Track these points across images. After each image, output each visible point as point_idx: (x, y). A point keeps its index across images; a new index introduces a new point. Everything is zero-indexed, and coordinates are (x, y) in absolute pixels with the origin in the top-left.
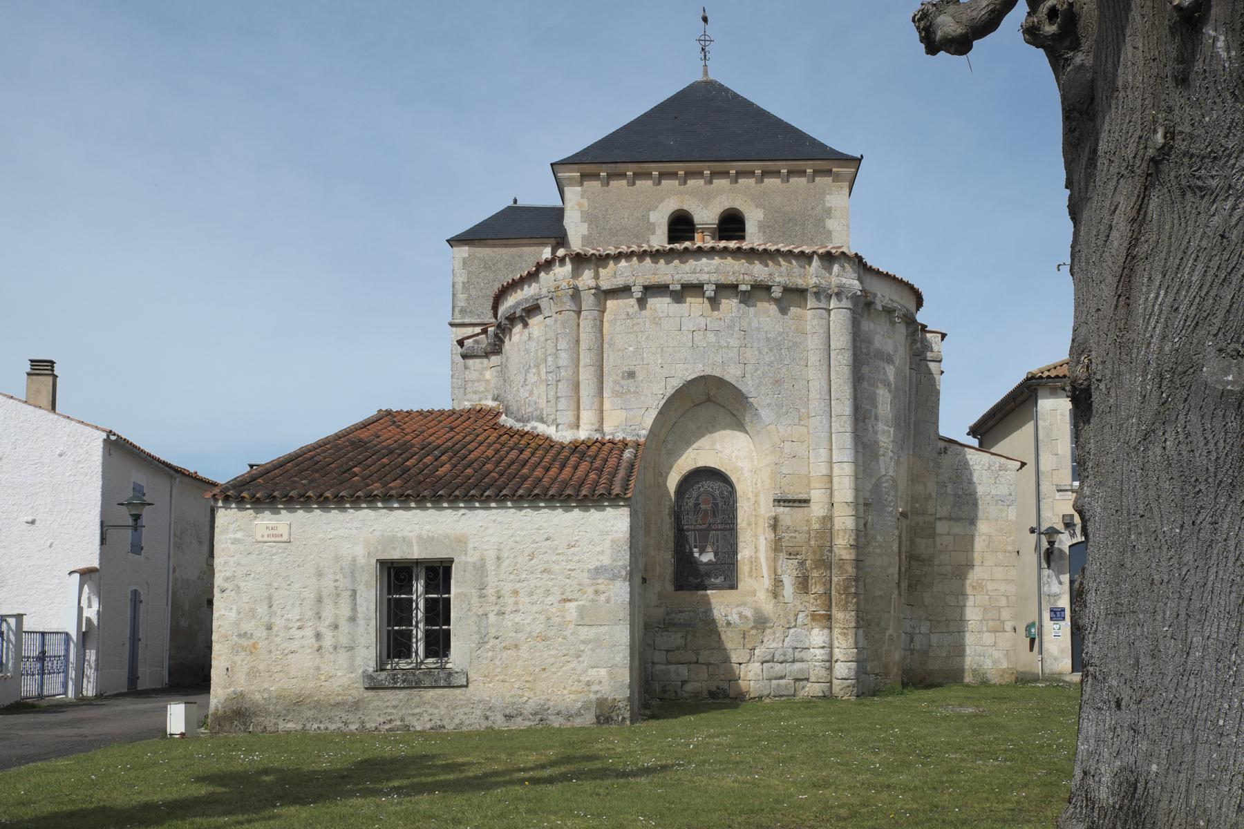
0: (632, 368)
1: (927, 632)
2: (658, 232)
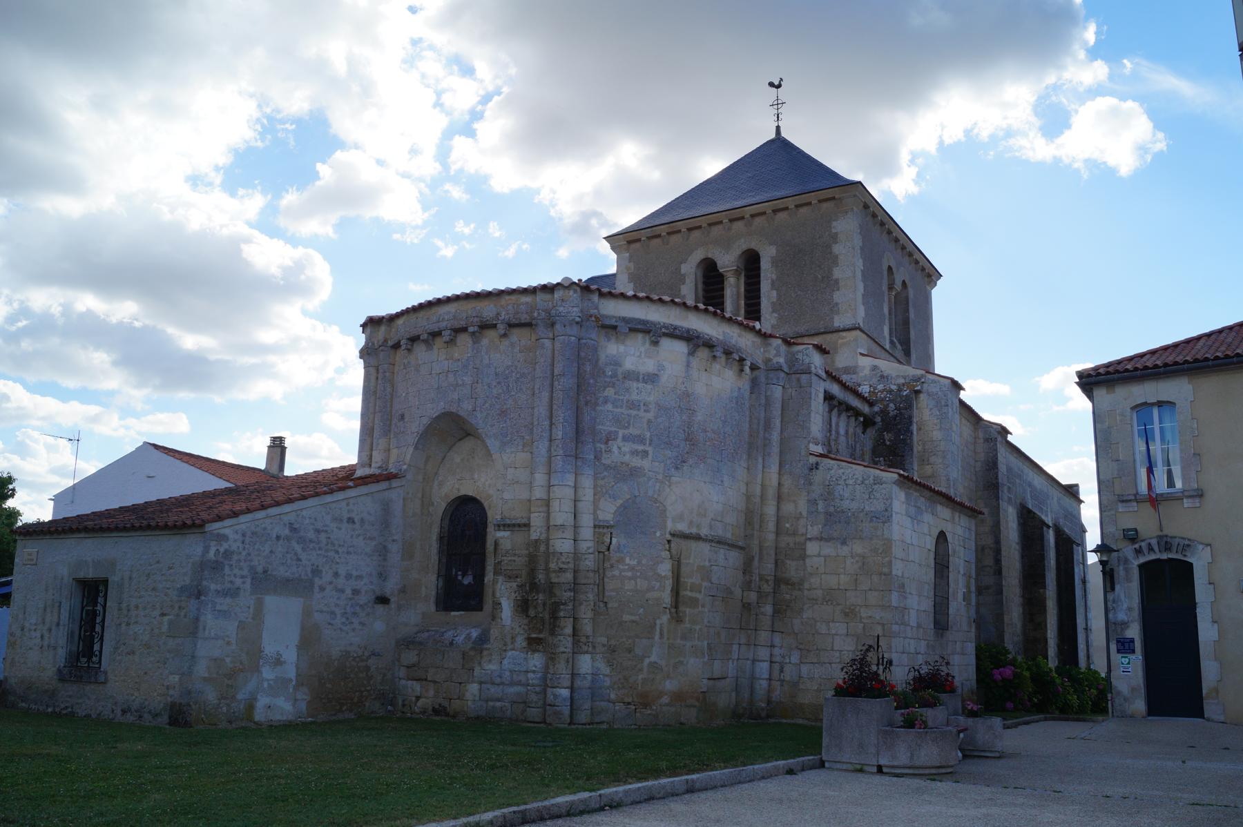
0: (403, 410)
1: (798, 662)
2: (688, 281)
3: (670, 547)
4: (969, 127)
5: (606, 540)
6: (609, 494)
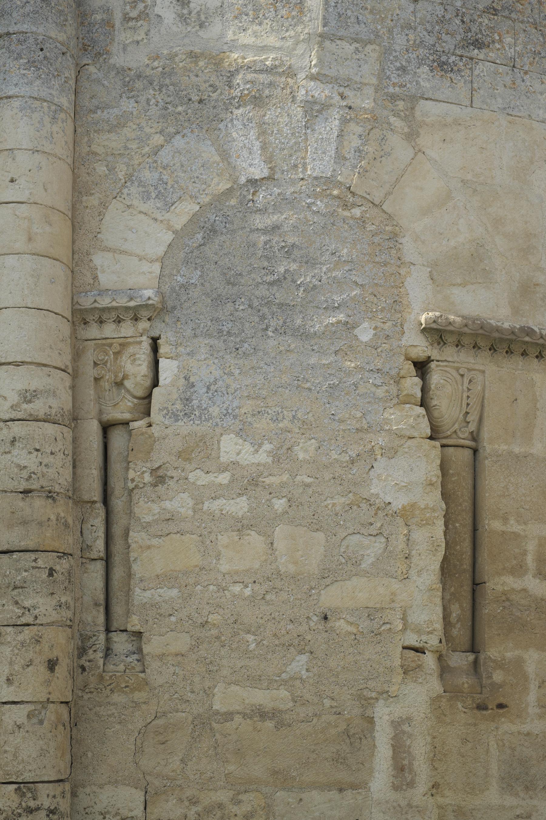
3: (424, 390)
4: (432, 358)
5: (129, 368)
6: (141, 184)
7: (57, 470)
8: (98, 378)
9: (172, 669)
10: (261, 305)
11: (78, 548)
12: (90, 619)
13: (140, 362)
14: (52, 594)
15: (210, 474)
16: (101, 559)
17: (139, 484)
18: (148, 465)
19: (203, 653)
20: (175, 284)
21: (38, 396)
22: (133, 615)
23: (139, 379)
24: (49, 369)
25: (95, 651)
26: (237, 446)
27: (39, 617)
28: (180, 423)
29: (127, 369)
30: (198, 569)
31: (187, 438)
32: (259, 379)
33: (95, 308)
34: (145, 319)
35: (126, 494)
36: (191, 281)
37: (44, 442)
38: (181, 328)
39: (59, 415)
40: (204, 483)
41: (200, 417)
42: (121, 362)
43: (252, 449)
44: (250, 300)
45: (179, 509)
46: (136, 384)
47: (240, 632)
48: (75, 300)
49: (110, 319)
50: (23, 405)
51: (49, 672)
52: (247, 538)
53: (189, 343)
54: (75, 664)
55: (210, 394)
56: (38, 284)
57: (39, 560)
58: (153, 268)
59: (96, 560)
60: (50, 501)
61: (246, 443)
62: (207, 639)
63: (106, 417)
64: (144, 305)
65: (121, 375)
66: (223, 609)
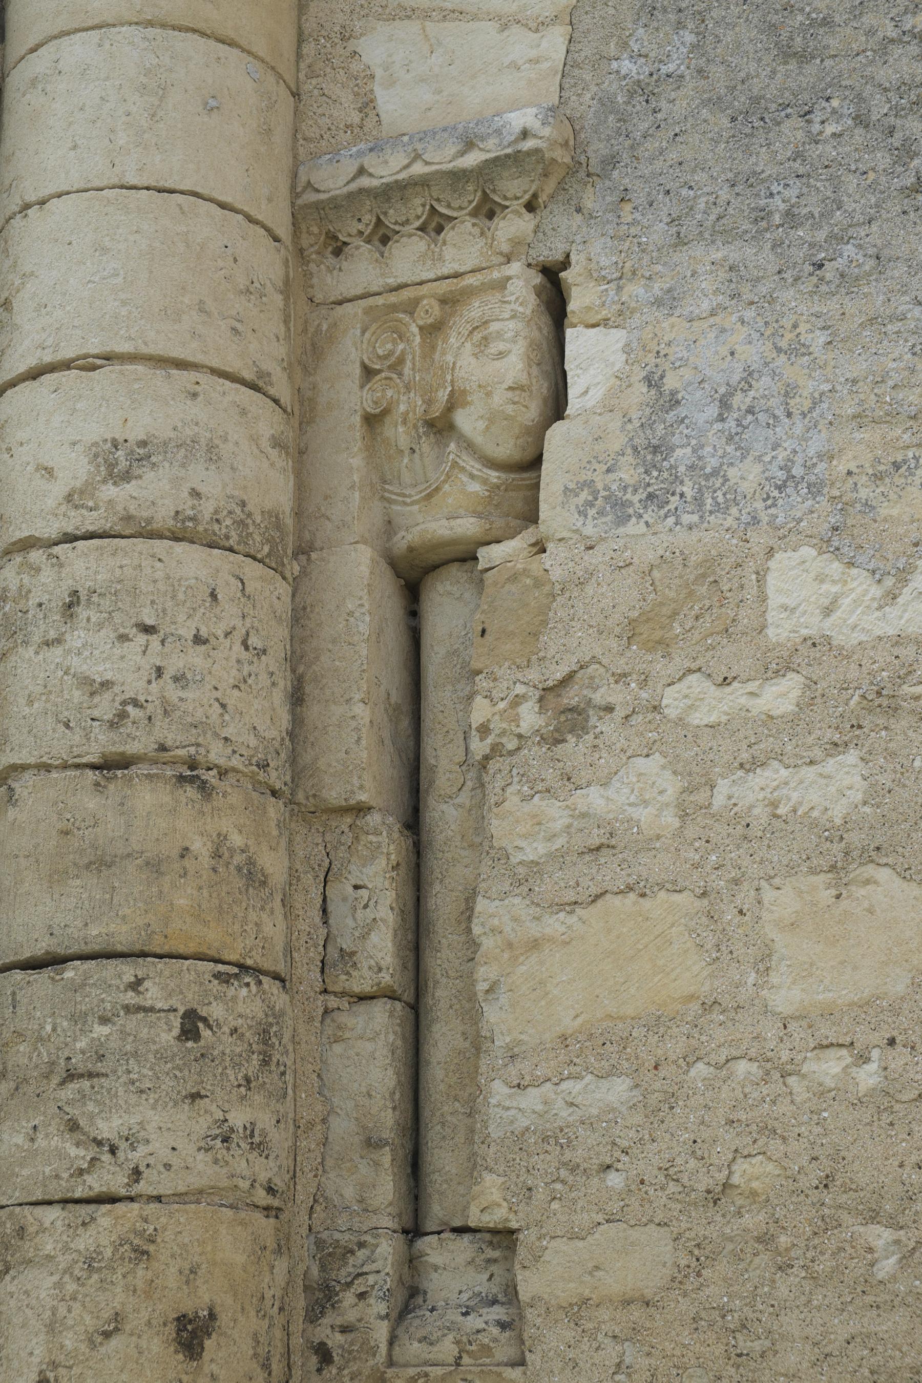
7: (218, 694)
8: (375, 416)
9: (611, 1352)
10: (897, 111)
11: (312, 960)
12: (349, 1192)
13: (502, 346)
14: (195, 1096)
15: (735, 684)
16: (392, 996)
17: (504, 740)
18: (533, 675)
19: (714, 1293)
20: (615, 86)
21: (153, 459)
22: (485, 1174)
23: (499, 398)
24: (193, 376)
25: (362, 1296)
26: (825, 587)
27: (146, 1173)
28: (634, 528)
29: (462, 374)
30: (695, 1007)
31: (656, 574)
32: (896, 355)
33: (361, 191)
34: (517, 205)
35: (469, 784)
36: (664, 69)
37: (169, 604)
38: (635, 222)
39: (228, 522)
40: (713, 719)
41: (699, 501)
42: (444, 353)
43: (876, 591)
44: (860, 98)
45: (630, 810)
46: (492, 419)
47: (845, 1217)
48: (303, 179)
49: (407, 222)
50: (104, 488)
51: (181, 1357)
52: (862, 892)
53: (659, 268)
54: (297, 1341)
55: (731, 424)
56: (161, 113)
57: (147, 984)
58: (544, 44)
59: (372, 998)
60: (191, 791)
61: (854, 571)
62: (730, 1246)
63: (402, 541)
64: (508, 156)
65: (443, 396)
66: (784, 1139)
